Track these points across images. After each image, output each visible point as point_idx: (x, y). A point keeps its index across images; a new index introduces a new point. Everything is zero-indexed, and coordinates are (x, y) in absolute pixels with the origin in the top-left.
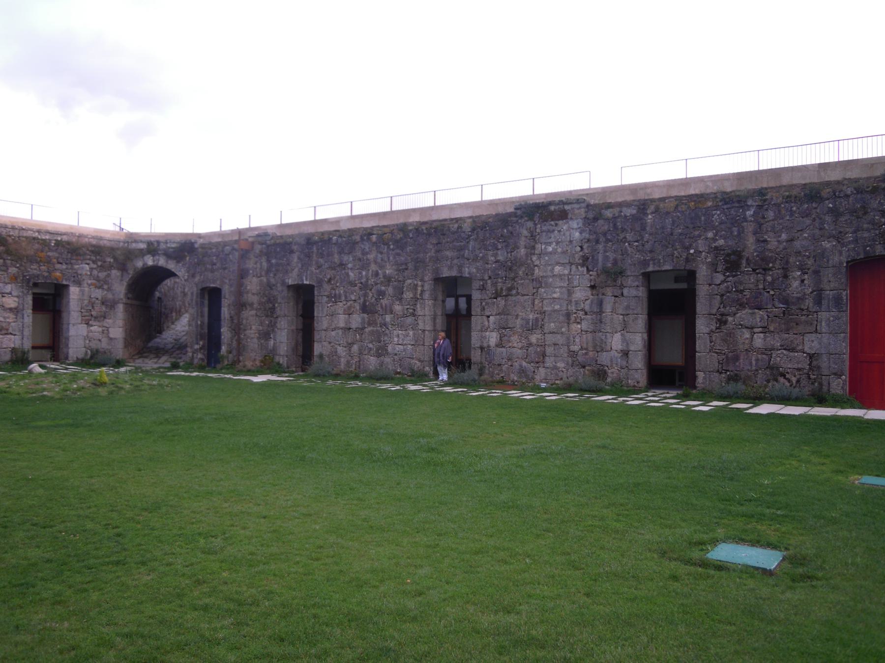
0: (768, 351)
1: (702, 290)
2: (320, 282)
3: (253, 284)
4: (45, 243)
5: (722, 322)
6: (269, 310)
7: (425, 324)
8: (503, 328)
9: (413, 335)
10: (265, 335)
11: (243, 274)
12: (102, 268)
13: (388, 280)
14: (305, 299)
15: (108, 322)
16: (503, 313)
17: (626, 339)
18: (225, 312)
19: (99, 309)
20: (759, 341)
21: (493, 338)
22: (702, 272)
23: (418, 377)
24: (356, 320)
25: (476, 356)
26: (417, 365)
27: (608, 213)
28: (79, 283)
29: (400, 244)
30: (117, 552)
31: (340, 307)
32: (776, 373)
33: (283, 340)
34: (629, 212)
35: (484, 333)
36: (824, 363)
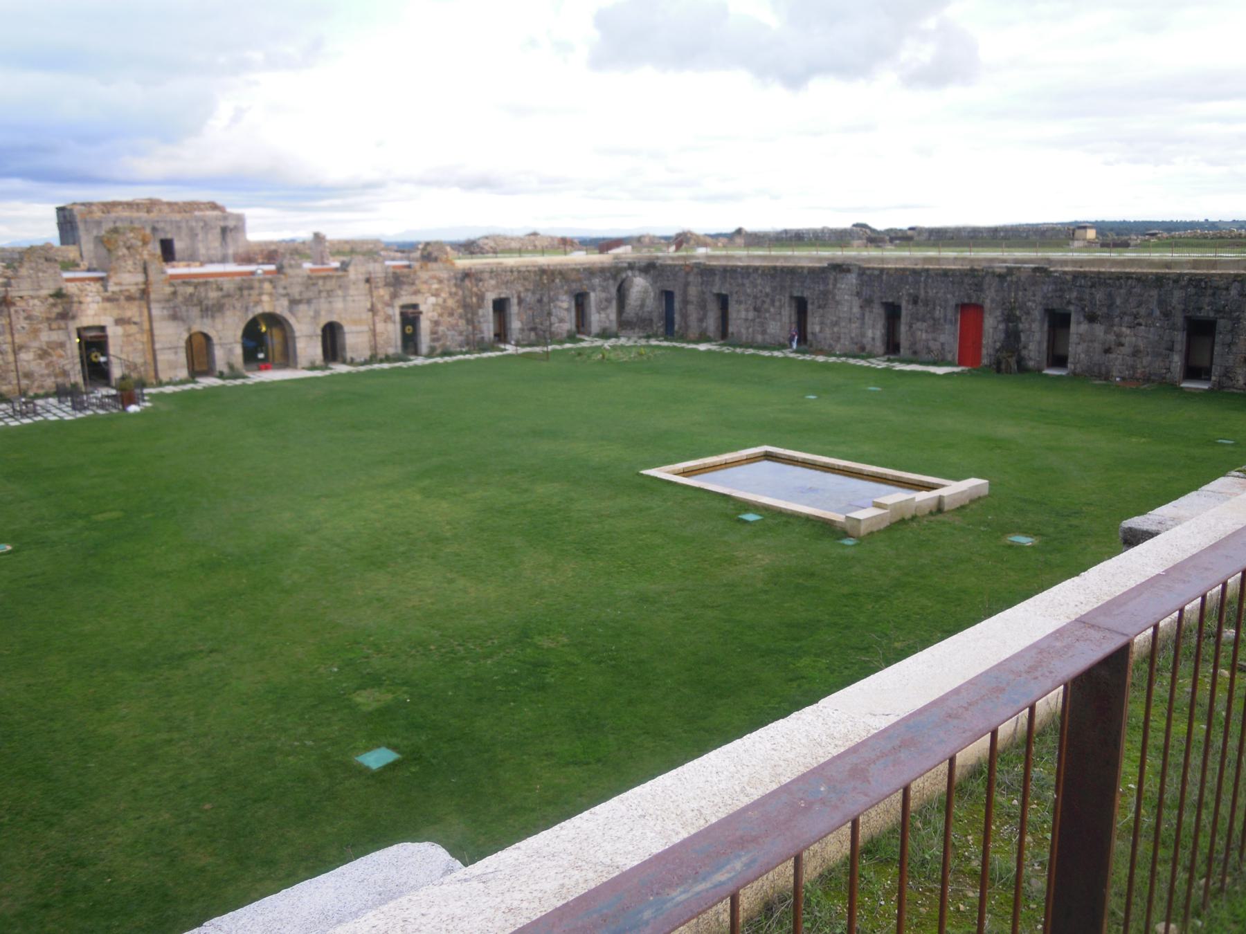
0: (927, 340)
1: (904, 312)
2: (731, 293)
3: (693, 291)
4: (578, 270)
5: (911, 327)
6: (703, 306)
7: (786, 319)
8: (822, 323)
9: (780, 322)
10: (701, 320)
11: (687, 284)
12: (605, 280)
13: (767, 295)
14: (723, 302)
15: (609, 311)
16: (822, 316)
17: (875, 333)
18: (677, 305)
19: (605, 304)
20: (924, 336)
21: (817, 329)
22: (904, 304)
23: (781, 347)
24: (751, 315)
25: (810, 337)
26: (782, 340)
27: (868, 272)
28: (594, 290)
29: (773, 277)
30: (455, 495)
31: (743, 307)
32: (929, 351)
33: (711, 323)
34: (876, 273)
35: (814, 326)
36: (947, 348)
